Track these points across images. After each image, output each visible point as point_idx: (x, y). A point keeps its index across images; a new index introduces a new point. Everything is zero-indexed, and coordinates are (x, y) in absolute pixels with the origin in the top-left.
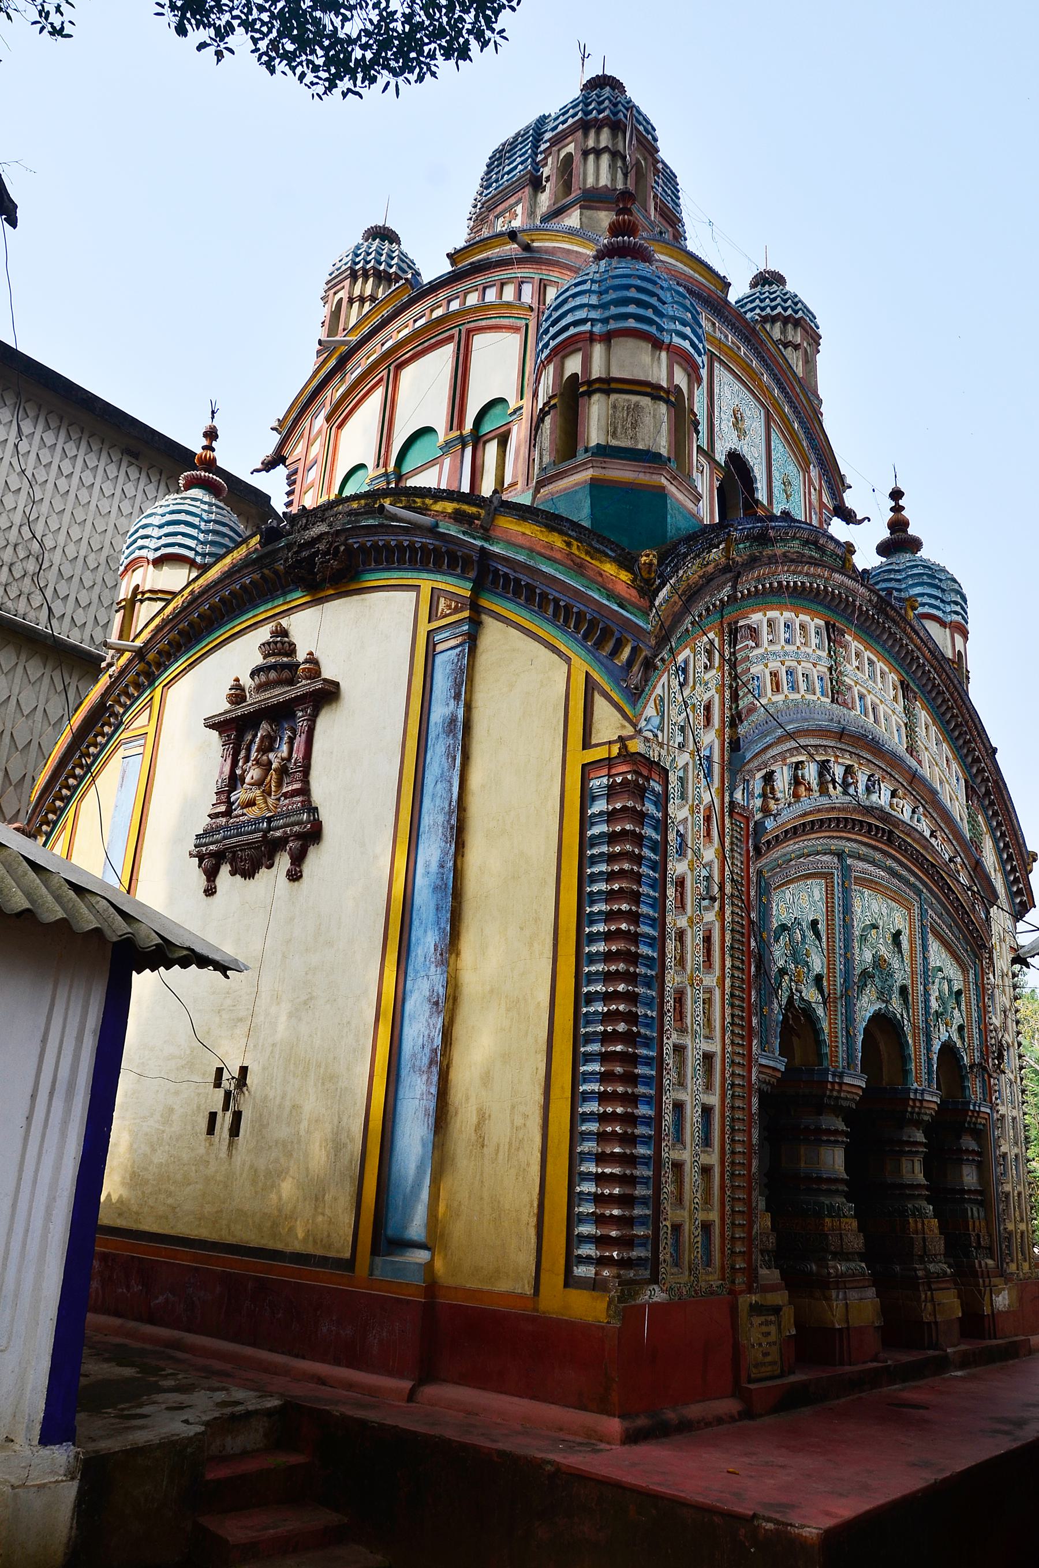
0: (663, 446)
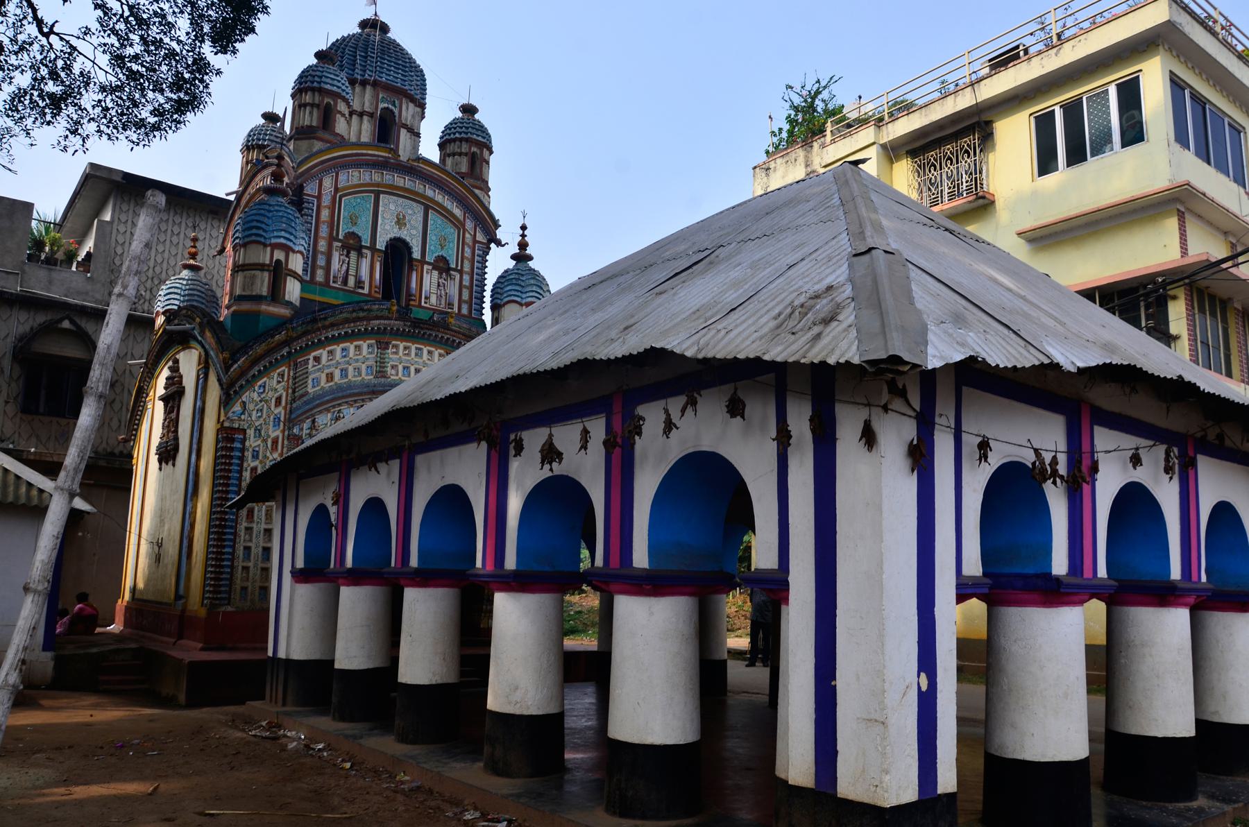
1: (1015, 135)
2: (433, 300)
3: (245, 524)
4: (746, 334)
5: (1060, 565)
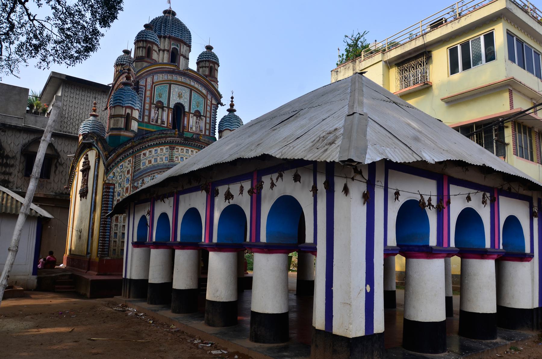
0: (122, 126)
1: (441, 57)
2: (194, 129)
5: (433, 241)
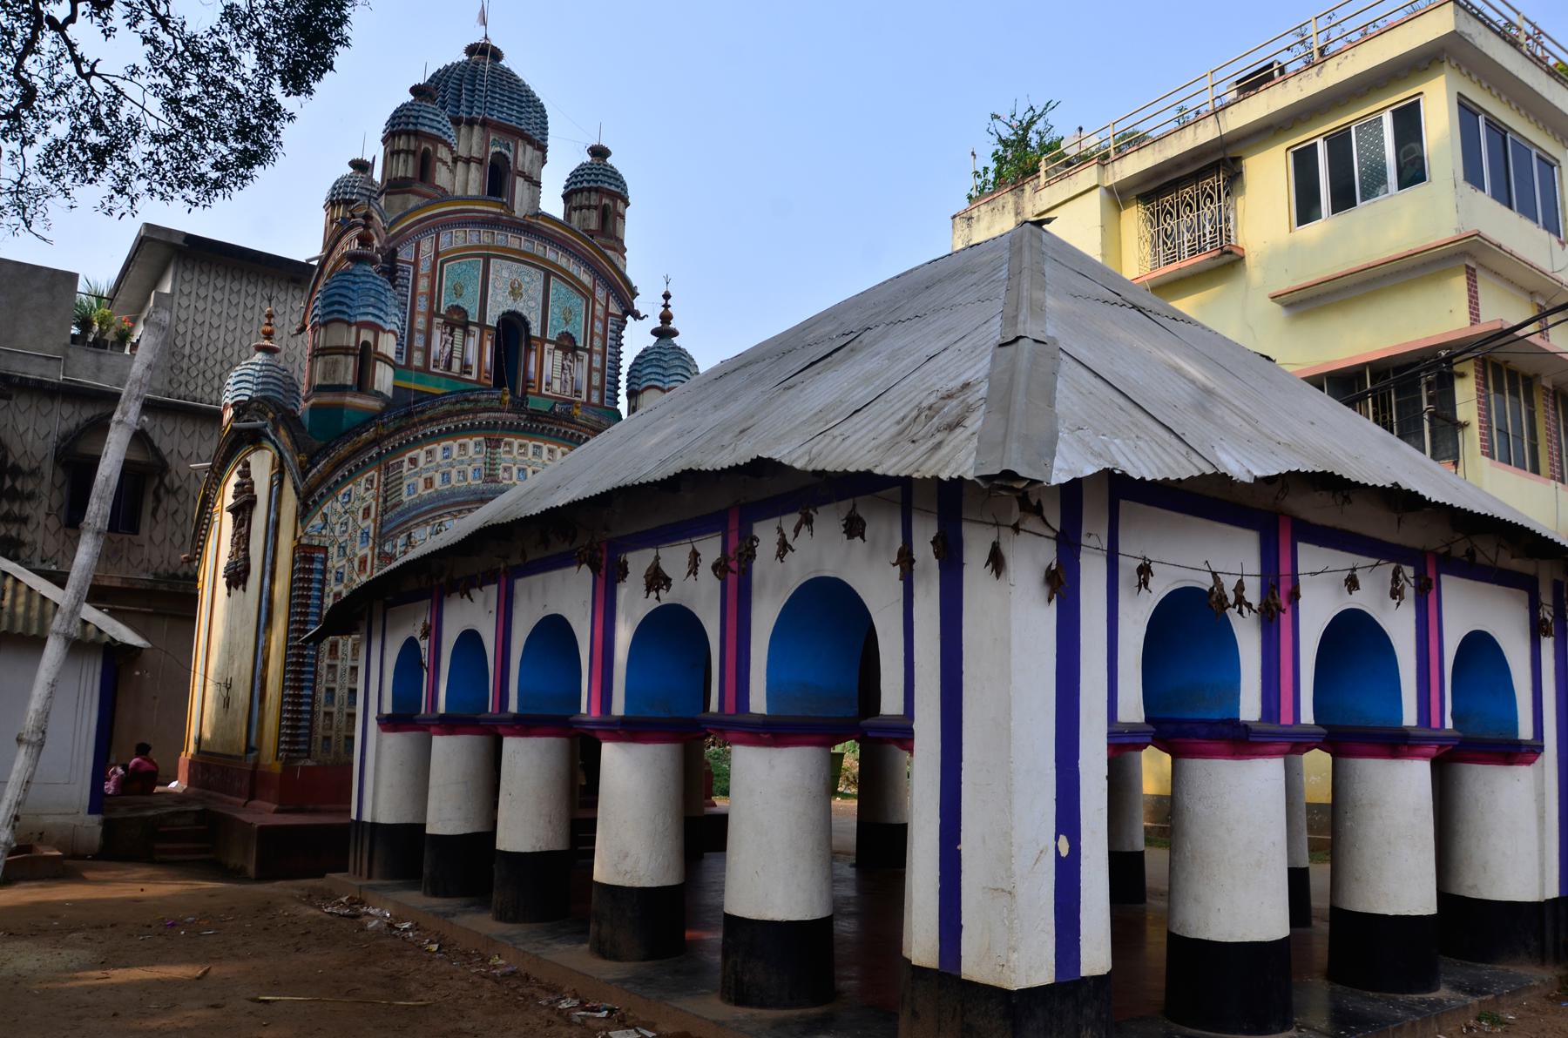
1: (1268, 176)
2: (557, 386)
3: (327, 661)
4: (860, 443)
5: (1250, 708)
